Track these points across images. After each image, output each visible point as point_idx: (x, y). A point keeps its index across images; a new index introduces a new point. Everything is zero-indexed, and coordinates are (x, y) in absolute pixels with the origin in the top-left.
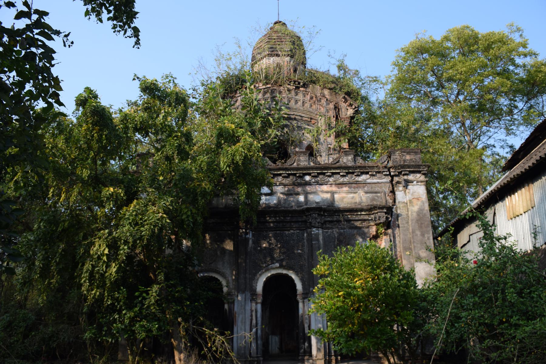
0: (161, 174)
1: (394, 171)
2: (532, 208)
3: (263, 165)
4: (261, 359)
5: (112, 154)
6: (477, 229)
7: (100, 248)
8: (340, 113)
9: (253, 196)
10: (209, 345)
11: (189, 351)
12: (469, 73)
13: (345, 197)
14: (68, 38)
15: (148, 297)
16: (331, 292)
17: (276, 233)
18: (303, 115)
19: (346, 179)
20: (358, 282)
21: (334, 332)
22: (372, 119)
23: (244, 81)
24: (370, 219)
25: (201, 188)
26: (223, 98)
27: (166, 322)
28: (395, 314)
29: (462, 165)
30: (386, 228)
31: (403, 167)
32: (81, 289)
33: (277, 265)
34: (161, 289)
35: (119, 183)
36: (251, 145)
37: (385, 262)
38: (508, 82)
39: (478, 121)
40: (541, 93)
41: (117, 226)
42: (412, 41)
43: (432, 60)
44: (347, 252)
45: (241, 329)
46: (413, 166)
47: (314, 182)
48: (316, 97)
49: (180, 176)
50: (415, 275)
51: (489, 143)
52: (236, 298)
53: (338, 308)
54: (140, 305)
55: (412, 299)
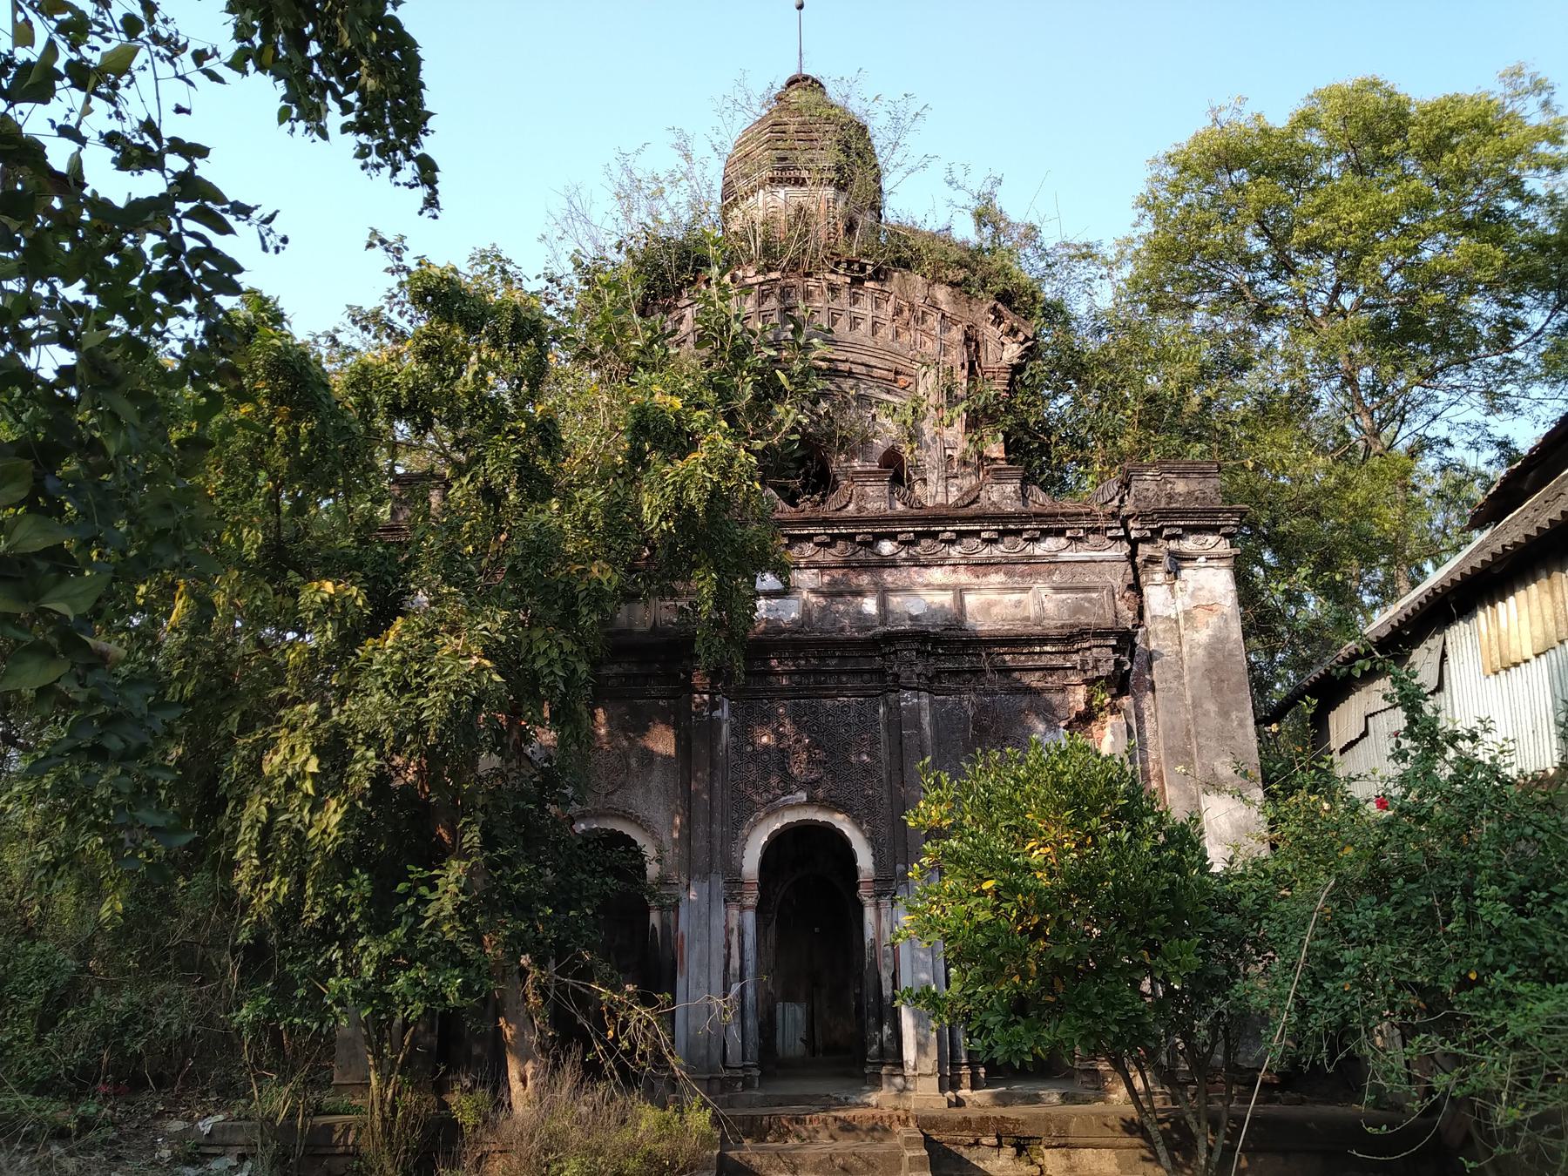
7: (292, 755)
8: (982, 354)
9: (735, 602)
10: (611, 1033)
13: (995, 601)
14: (273, 225)
18: (873, 362)
19: (998, 551)
21: (969, 996)
22: (1075, 368)
23: (703, 262)
27: (485, 968)
30: (1114, 691)
31: (1166, 514)
33: (802, 796)
34: (470, 873)
39: (1397, 370)
41: (343, 694)
43: (1260, 191)
45: (698, 985)
46: (1195, 511)
47: (905, 560)
48: (912, 308)
50: (1201, 833)
51: (1430, 433)
53: (979, 927)
54: (411, 920)
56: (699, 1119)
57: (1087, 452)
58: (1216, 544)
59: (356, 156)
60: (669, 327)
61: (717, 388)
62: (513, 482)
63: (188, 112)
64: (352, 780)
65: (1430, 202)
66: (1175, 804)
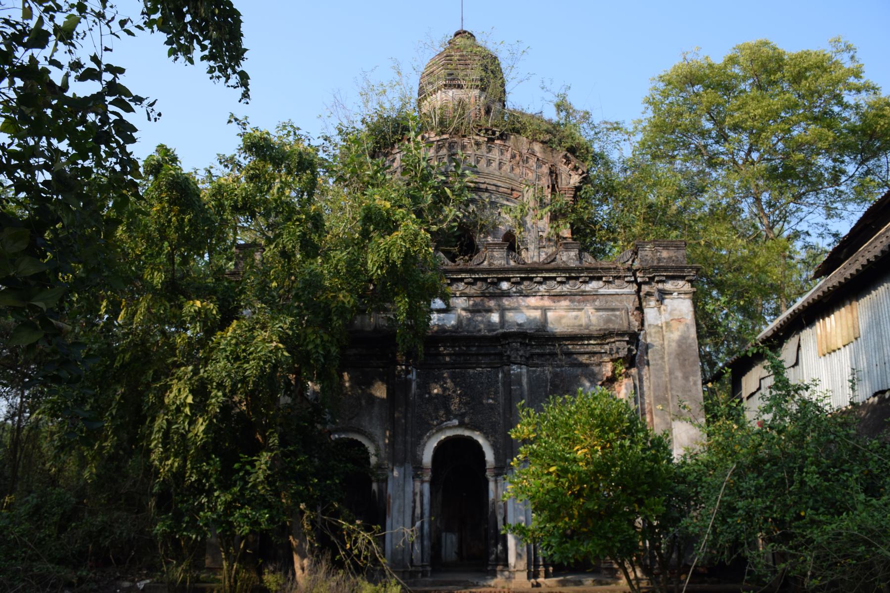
0: (274, 279)
1: (642, 275)
2: (856, 339)
3: (435, 265)
4: (429, 569)
5: (198, 249)
6: (765, 373)
7: (180, 393)
8: (559, 180)
9: (419, 315)
10: (348, 546)
11: (317, 555)
12: (767, 118)
13: (563, 316)
14: (154, 107)
15: (253, 471)
16: (538, 467)
18: (499, 184)
19: (566, 288)
20: (579, 452)
21: (542, 529)
22: (609, 190)
23: (406, 129)
25: (338, 302)
26: (373, 157)
28: (636, 502)
29: (753, 266)
30: (627, 365)
31: (657, 269)
32: (150, 457)
34: (273, 459)
35: (209, 294)
36: (416, 235)
37: (622, 421)
38: (831, 134)
39: (781, 194)
40: (883, 149)
41: (206, 361)
43: (709, 96)
45: (398, 522)
46: (672, 268)
48: (521, 155)
49: (303, 283)
50: (669, 441)
51: (799, 228)
52: (390, 474)
53: (548, 491)
54: (242, 483)
55: (664, 479)
57: (616, 235)
58: (683, 285)
60: (387, 163)
61: (413, 197)
62: (298, 247)
63: (111, 50)
65: (796, 105)
66: (657, 426)
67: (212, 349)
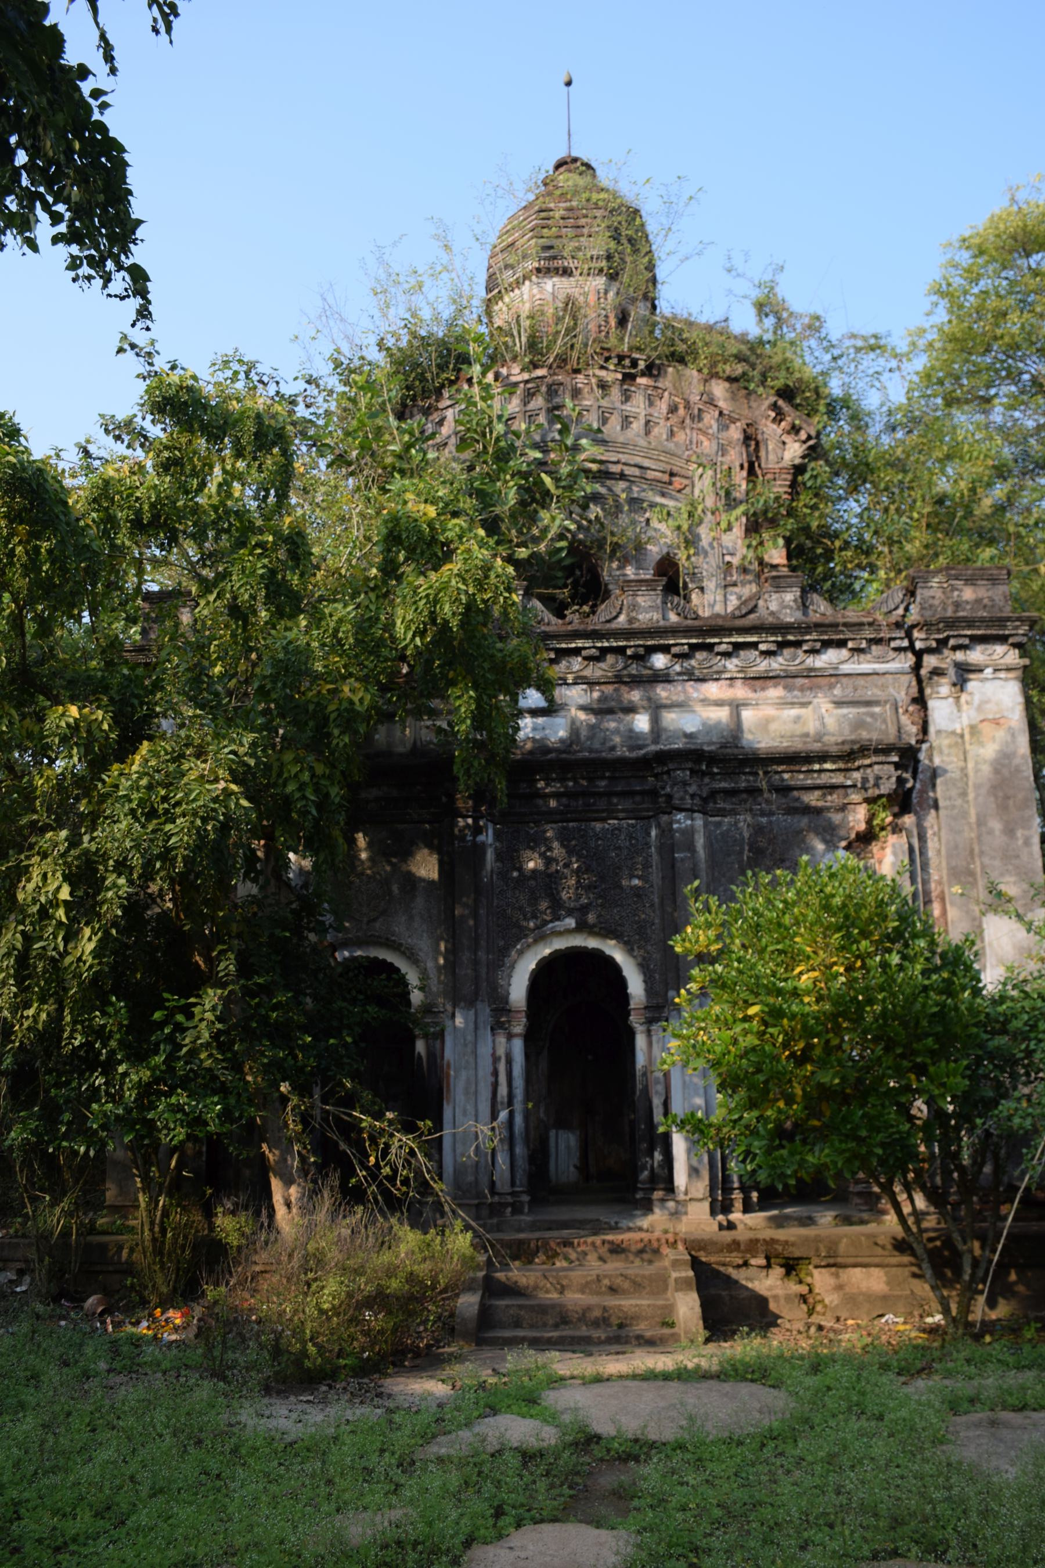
0: (218, 658)
1: (923, 636)
7: (45, 882)
9: (497, 722)
10: (372, 1159)
13: (773, 717)
15: (190, 1024)
17: (564, 828)
18: (646, 463)
19: (776, 664)
20: (804, 977)
21: (735, 1121)
22: (860, 472)
23: (464, 359)
24: (849, 783)
25: (341, 701)
26: (400, 416)
27: (245, 1095)
30: (896, 809)
31: (952, 623)
33: (571, 922)
34: (226, 1001)
36: (487, 568)
37: (885, 918)
41: (93, 820)
42: (997, 211)
44: (774, 889)
45: (465, 1113)
46: (982, 620)
47: (679, 674)
48: (688, 406)
49: (273, 666)
52: (448, 1023)
54: (169, 1048)
56: (461, 1242)
58: (1005, 655)
59: (67, 268)
60: (430, 428)
64: (105, 908)
66: (952, 922)
67: (103, 798)
